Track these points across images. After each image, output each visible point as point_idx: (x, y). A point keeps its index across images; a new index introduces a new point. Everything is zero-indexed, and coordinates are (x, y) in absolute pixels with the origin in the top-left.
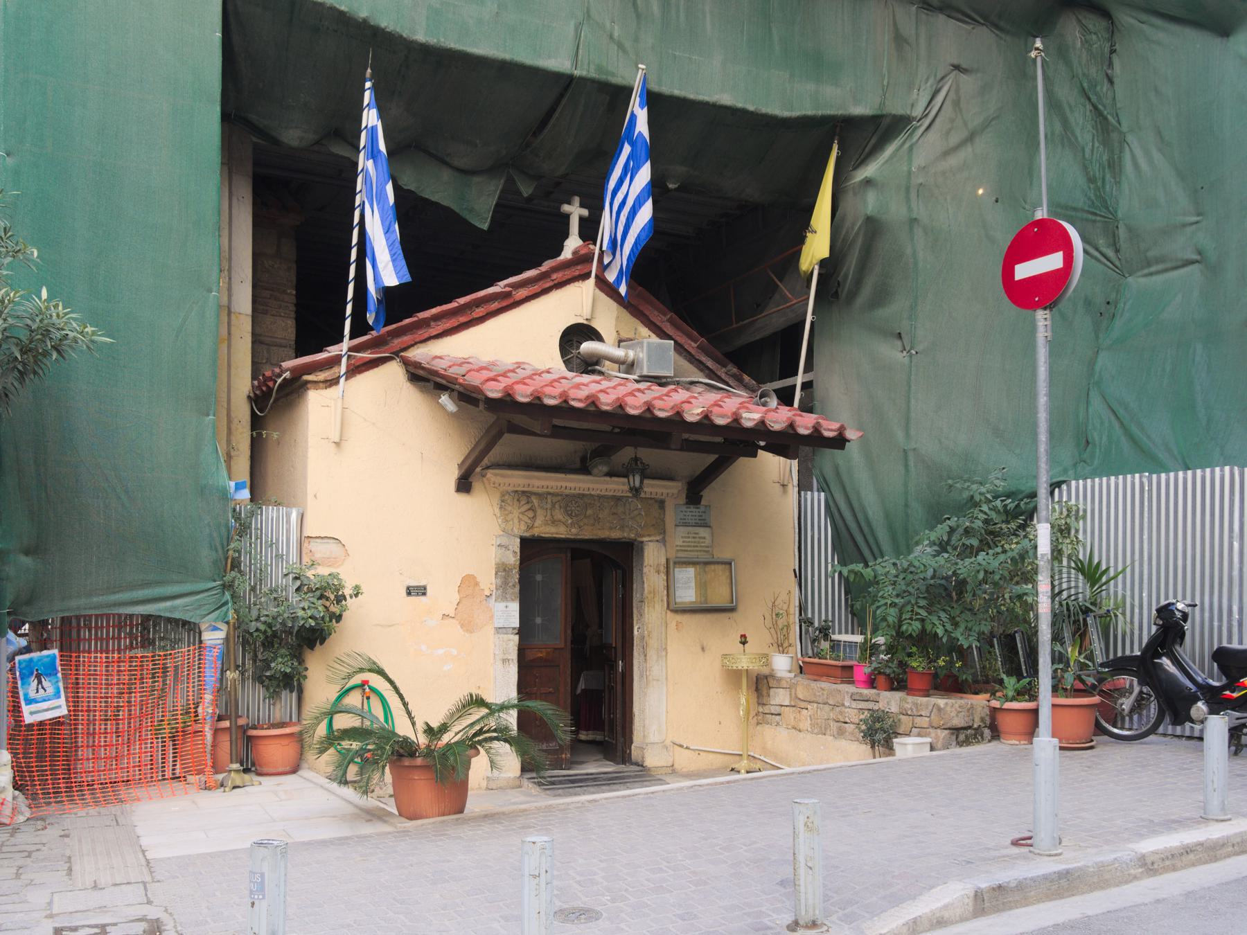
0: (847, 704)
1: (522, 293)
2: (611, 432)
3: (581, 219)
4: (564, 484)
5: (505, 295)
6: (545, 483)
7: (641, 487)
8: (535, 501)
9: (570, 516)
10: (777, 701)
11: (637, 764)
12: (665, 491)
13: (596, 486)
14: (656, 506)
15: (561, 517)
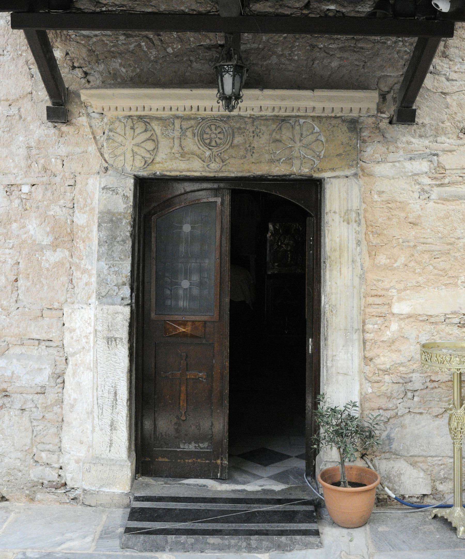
4: (195, 104)
6: (167, 103)
8: (157, 127)
15: (195, 148)
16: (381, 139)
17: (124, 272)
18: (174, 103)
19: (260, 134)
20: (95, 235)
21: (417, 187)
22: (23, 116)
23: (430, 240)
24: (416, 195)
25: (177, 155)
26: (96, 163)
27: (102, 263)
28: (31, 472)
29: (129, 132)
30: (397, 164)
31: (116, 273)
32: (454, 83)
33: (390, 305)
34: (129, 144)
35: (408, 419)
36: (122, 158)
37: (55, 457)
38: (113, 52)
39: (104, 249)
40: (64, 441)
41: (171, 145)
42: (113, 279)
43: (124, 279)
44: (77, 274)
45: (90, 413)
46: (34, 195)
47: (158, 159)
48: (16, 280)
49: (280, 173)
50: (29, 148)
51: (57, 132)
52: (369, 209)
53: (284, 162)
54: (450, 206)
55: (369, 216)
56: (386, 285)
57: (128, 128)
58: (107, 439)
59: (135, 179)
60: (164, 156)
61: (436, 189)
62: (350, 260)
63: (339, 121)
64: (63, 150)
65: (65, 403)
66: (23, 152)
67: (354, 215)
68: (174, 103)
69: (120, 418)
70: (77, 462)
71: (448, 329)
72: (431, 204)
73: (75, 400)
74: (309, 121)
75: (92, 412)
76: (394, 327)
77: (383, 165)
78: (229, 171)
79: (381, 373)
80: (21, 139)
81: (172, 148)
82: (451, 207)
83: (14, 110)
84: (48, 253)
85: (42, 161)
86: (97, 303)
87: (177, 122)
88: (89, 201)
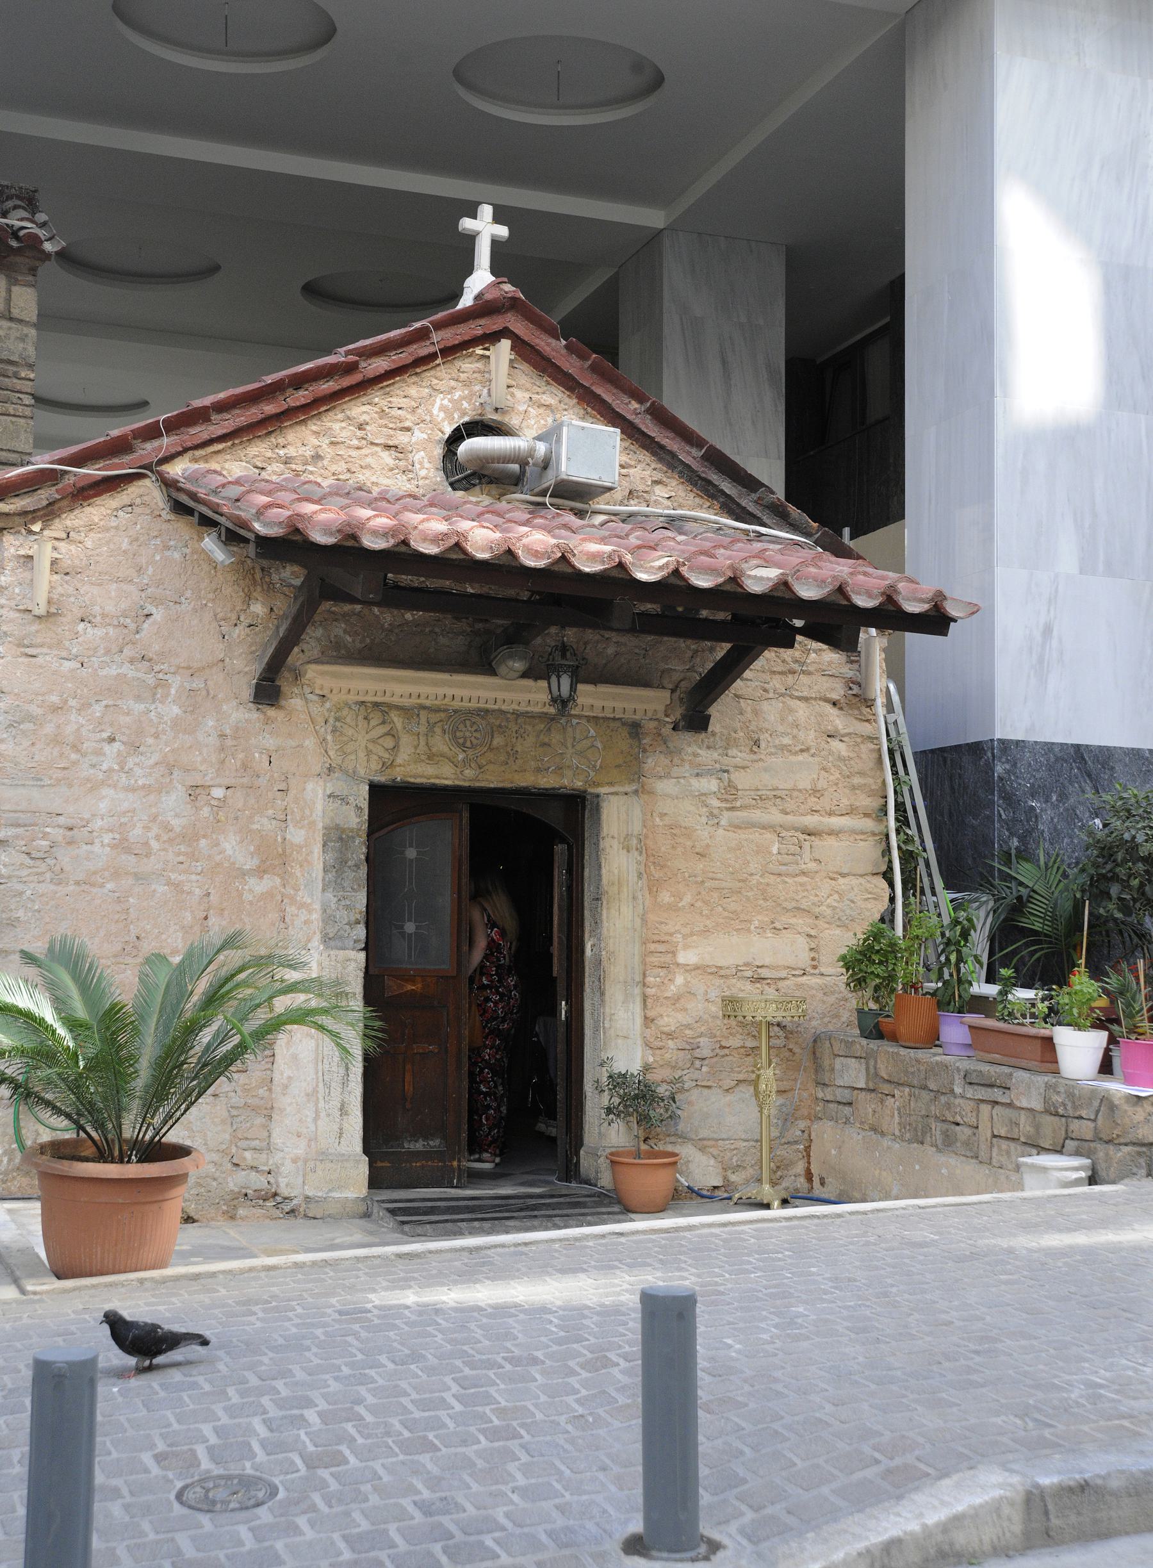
0: (958, 1090)
1: (380, 364)
2: (529, 601)
3: (495, 243)
4: (449, 692)
5: (351, 368)
7: (571, 698)
8: (397, 720)
9: (463, 747)
10: (845, 1080)
11: (587, 1182)
12: (640, 707)
13: (507, 696)
14: (624, 732)
15: (446, 749)
16: (663, 748)
17: (358, 906)
18: (425, 690)
19: (525, 735)
20: (317, 858)
21: (705, 809)
22: (212, 692)
23: (719, 876)
24: (704, 820)
25: (423, 757)
26: (316, 764)
27: (329, 895)
28: (229, 1179)
29: (362, 723)
30: (682, 781)
31: (347, 907)
32: (749, 683)
33: (674, 953)
34: (362, 740)
35: (694, 1095)
36: (353, 757)
37: (264, 1156)
38: (333, 613)
39: (331, 876)
40: (274, 1135)
41: (415, 743)
42: (344, 916)
43: (358, 916)
44: (291, 910)
45: (312, 1095)
46: (230, 801)
47: (399, 761)
48: (206, 918)
49: (548, 786)
50: (223, 736)
51: (262, 716)
52: (651, 836)
53: (554, 772)
54: (743, 835)
55: (650, 843)
56: (670, 928)
57: (360, 718)
58: (336, 1127)
59: (370, 786)
60: (407, 757)
61: (726, 814)
62: (631, 896)
63: (618, 724)
64: (270, 742)
65: (274, 1082)
66: (213, 740)
67: (634, 842)
68: (425, 690)
69: (352, 1098)
70: (294, 1161)
71: (739, 984)
72: (721, 831)
73: (290, 1078)
74: (584, 721)
75: (315, 1091)
76: (680, 980)
77: (666, 781)
78: (487, 780)
79: (664, 1036)
80: (211, 723)
81: (416, 747)
82: (743, 836)
83: (198, 684)
84: (252, 881)
85: (241, 756)
86: (322, 947)
87: (423, 713)
88: (307, 812)
